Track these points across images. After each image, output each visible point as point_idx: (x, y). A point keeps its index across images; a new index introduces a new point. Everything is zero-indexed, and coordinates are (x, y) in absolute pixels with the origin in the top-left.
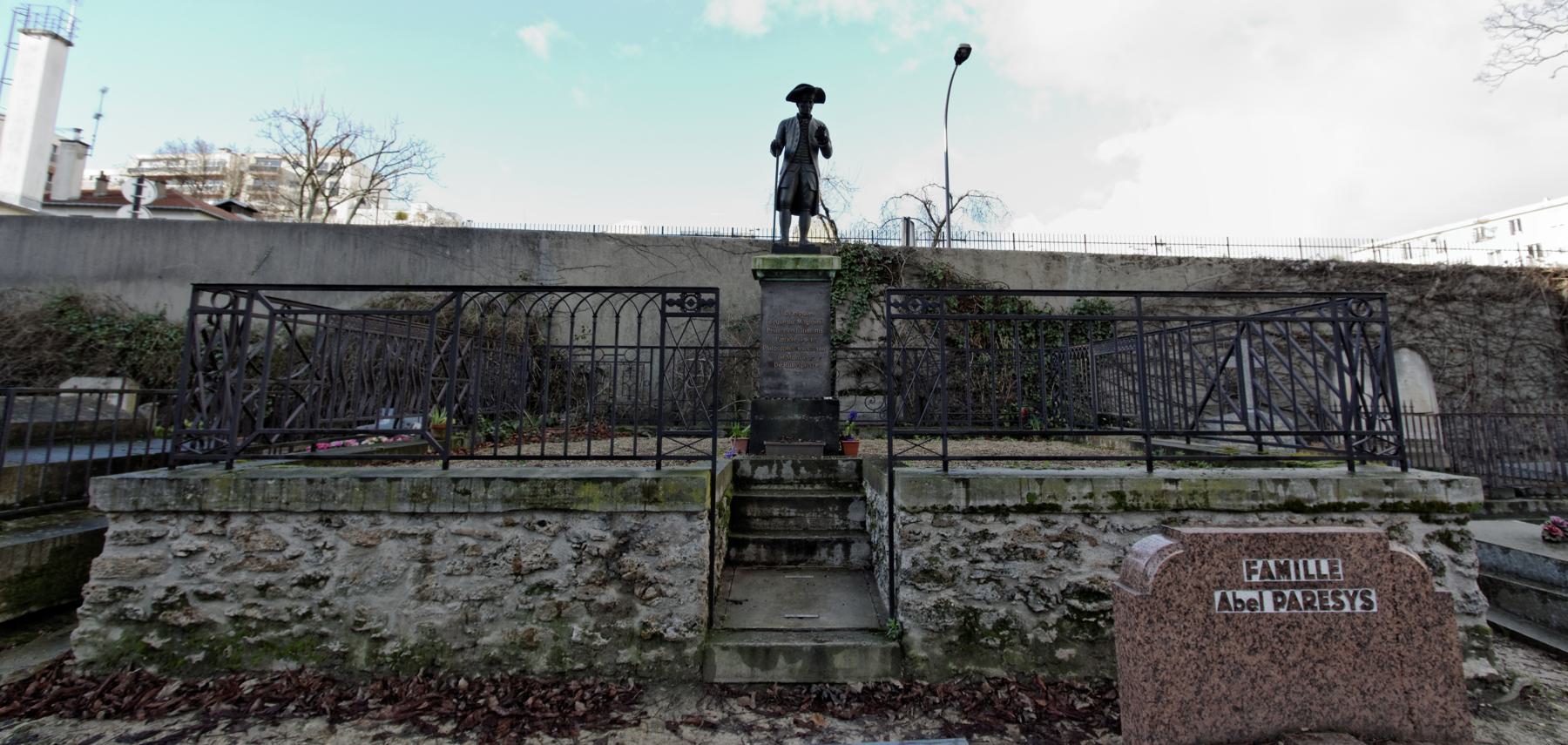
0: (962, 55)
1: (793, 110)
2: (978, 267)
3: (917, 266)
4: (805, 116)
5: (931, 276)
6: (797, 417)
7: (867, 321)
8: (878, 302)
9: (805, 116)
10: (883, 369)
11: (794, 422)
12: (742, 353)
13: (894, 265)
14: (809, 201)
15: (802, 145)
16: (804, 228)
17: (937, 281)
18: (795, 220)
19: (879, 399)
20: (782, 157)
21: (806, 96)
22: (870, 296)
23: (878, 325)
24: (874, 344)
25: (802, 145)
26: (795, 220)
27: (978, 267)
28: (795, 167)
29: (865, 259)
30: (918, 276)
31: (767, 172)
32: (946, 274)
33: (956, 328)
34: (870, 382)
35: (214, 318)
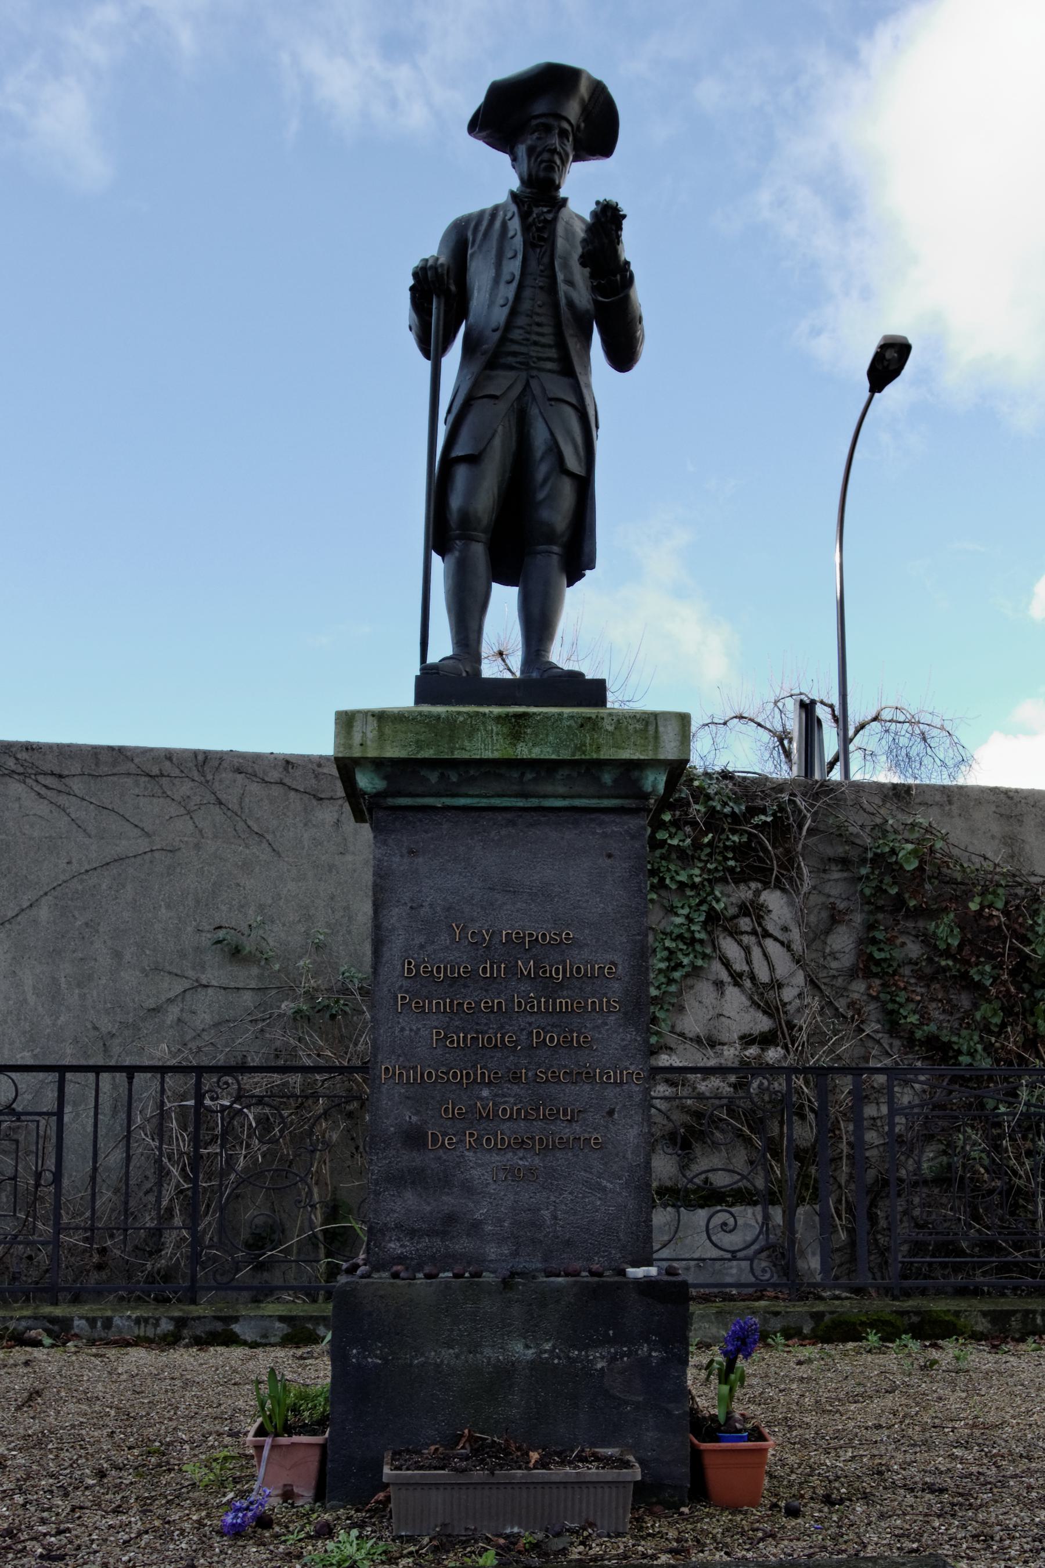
0: (889, 362)
1: (492, 178)
2: (1010, 840)
3: (841, 835)
4: (539, 195)
5: (884, 863)
6: (521, 1351)
7: (705, 990)
8: (734, 933)
9: (539, 195)
10: (759, 1127)
11: (505, 1372)
12: (338, 1085)
13: (780, 829)
14: (558, 515)
15: (527, 334)
16: (538, 624)
17: (895, 870)
18: (504, 602)
19: (749, 1216)
20: (453, 359)
21: (545, 115)
22: (713, 918)
23: (735, 999)
24: (730, 1055)
25: (527, 334)
26: (504, 602)
27: (1010, 840)
28: (502, 382)
29: (697, 809)
30: (844, 862)
31: (388, 410)
32: (925, 855)
33: (951, 1009)
34: (719, 1165)
35: (885, 1091)
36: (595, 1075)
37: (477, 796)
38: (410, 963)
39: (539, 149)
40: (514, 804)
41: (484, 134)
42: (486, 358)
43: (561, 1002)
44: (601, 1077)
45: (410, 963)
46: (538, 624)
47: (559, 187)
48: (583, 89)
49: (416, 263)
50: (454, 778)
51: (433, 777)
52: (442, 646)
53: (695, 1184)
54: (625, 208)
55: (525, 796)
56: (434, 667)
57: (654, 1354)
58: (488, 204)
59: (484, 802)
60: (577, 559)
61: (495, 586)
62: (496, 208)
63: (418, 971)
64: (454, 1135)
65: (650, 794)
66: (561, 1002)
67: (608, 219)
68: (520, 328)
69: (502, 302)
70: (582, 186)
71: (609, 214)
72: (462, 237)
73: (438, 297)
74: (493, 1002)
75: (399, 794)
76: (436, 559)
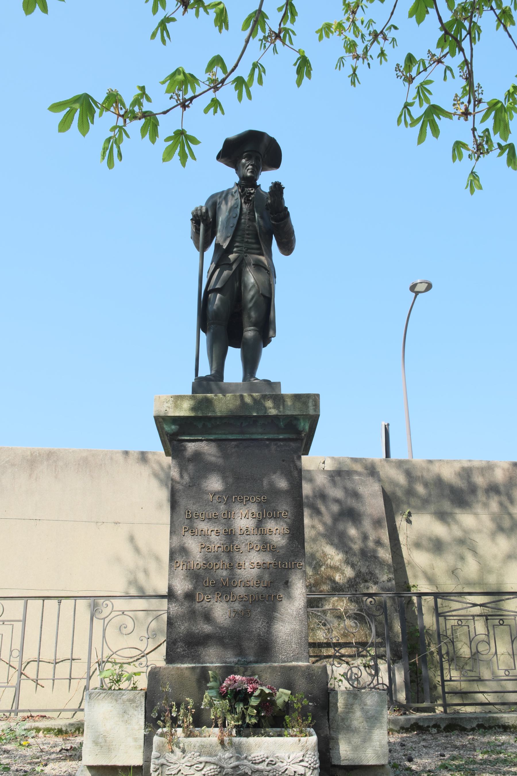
9: (248, 183)
16: (250, 363)
18: (234, 356)
26: (234, 356)
31: (184, 271)
36: (278, 565)
37: (221, 434)
38: (188, 512)
39: (247, 165)
40: (238, 438)
41: (222, 160)
42: (221, 259)
43: (261, 530)
44: (281, 566)
45: (188, 512)
46: (250, 363)
47: (256, 180)
48: (265, 140)
49: (193, 209)
50: (209, 425)
51: (200, 426)
52: (205, 370)
53: (340, 653)
54: (283, 184)
55: (242, 433)
56: (202, 378)
57: (310, 704)
58: (225, 189)
59: (224, 437)
60: (266, 329)
61: (230, 349)
62: (229, 190)
63: (192, 515)
64: (210, 594)
65: (302, 431)
66: (261, 530)
67: (277, 189)
68: (239, 236)
69: (234, 216)
70: (265, 180)
71: (277, 186)
72: (214, 203)
73: (204, 223)
74: (229, 530)
75: (184, 434)
76: (202, 333)
